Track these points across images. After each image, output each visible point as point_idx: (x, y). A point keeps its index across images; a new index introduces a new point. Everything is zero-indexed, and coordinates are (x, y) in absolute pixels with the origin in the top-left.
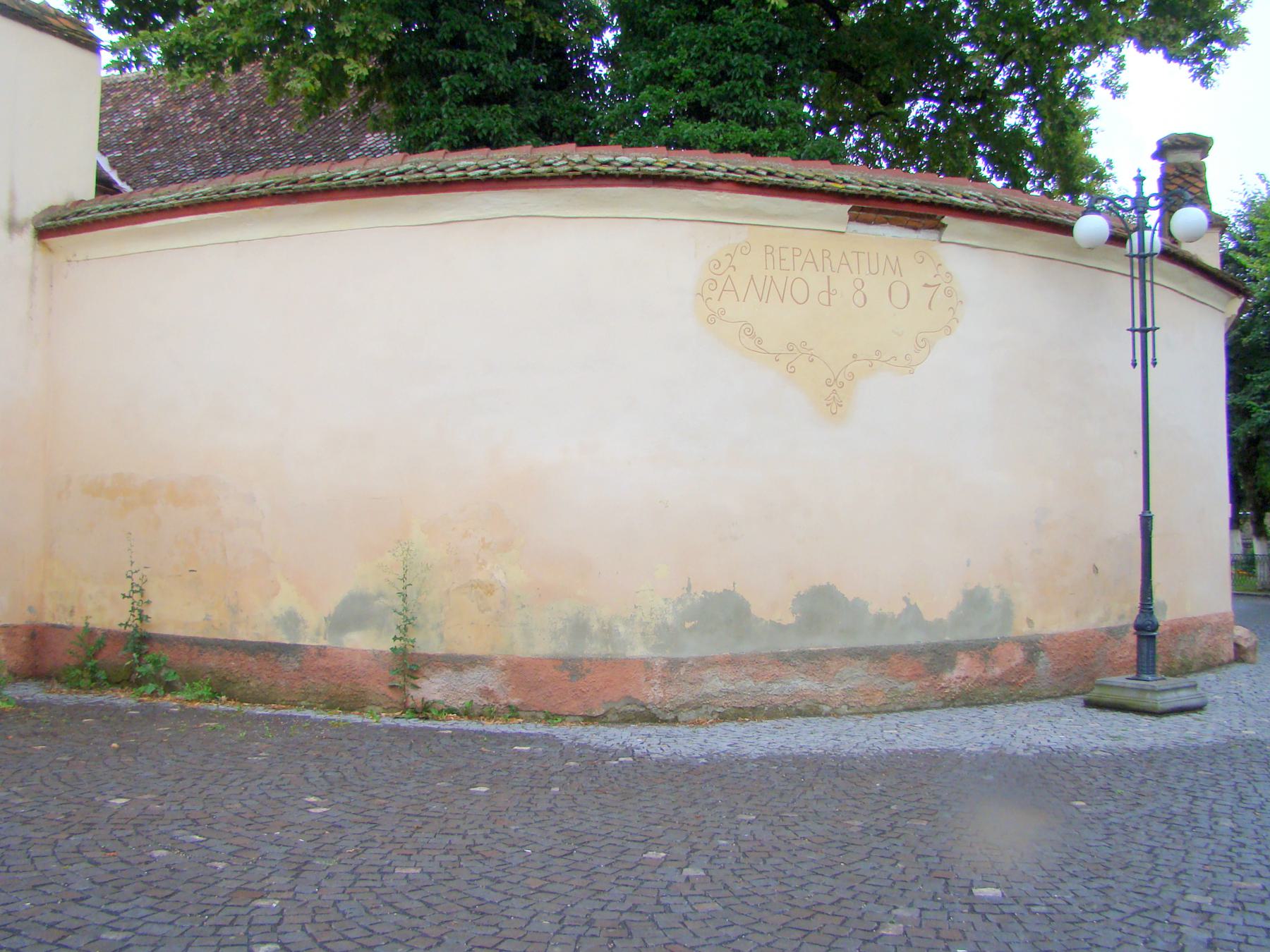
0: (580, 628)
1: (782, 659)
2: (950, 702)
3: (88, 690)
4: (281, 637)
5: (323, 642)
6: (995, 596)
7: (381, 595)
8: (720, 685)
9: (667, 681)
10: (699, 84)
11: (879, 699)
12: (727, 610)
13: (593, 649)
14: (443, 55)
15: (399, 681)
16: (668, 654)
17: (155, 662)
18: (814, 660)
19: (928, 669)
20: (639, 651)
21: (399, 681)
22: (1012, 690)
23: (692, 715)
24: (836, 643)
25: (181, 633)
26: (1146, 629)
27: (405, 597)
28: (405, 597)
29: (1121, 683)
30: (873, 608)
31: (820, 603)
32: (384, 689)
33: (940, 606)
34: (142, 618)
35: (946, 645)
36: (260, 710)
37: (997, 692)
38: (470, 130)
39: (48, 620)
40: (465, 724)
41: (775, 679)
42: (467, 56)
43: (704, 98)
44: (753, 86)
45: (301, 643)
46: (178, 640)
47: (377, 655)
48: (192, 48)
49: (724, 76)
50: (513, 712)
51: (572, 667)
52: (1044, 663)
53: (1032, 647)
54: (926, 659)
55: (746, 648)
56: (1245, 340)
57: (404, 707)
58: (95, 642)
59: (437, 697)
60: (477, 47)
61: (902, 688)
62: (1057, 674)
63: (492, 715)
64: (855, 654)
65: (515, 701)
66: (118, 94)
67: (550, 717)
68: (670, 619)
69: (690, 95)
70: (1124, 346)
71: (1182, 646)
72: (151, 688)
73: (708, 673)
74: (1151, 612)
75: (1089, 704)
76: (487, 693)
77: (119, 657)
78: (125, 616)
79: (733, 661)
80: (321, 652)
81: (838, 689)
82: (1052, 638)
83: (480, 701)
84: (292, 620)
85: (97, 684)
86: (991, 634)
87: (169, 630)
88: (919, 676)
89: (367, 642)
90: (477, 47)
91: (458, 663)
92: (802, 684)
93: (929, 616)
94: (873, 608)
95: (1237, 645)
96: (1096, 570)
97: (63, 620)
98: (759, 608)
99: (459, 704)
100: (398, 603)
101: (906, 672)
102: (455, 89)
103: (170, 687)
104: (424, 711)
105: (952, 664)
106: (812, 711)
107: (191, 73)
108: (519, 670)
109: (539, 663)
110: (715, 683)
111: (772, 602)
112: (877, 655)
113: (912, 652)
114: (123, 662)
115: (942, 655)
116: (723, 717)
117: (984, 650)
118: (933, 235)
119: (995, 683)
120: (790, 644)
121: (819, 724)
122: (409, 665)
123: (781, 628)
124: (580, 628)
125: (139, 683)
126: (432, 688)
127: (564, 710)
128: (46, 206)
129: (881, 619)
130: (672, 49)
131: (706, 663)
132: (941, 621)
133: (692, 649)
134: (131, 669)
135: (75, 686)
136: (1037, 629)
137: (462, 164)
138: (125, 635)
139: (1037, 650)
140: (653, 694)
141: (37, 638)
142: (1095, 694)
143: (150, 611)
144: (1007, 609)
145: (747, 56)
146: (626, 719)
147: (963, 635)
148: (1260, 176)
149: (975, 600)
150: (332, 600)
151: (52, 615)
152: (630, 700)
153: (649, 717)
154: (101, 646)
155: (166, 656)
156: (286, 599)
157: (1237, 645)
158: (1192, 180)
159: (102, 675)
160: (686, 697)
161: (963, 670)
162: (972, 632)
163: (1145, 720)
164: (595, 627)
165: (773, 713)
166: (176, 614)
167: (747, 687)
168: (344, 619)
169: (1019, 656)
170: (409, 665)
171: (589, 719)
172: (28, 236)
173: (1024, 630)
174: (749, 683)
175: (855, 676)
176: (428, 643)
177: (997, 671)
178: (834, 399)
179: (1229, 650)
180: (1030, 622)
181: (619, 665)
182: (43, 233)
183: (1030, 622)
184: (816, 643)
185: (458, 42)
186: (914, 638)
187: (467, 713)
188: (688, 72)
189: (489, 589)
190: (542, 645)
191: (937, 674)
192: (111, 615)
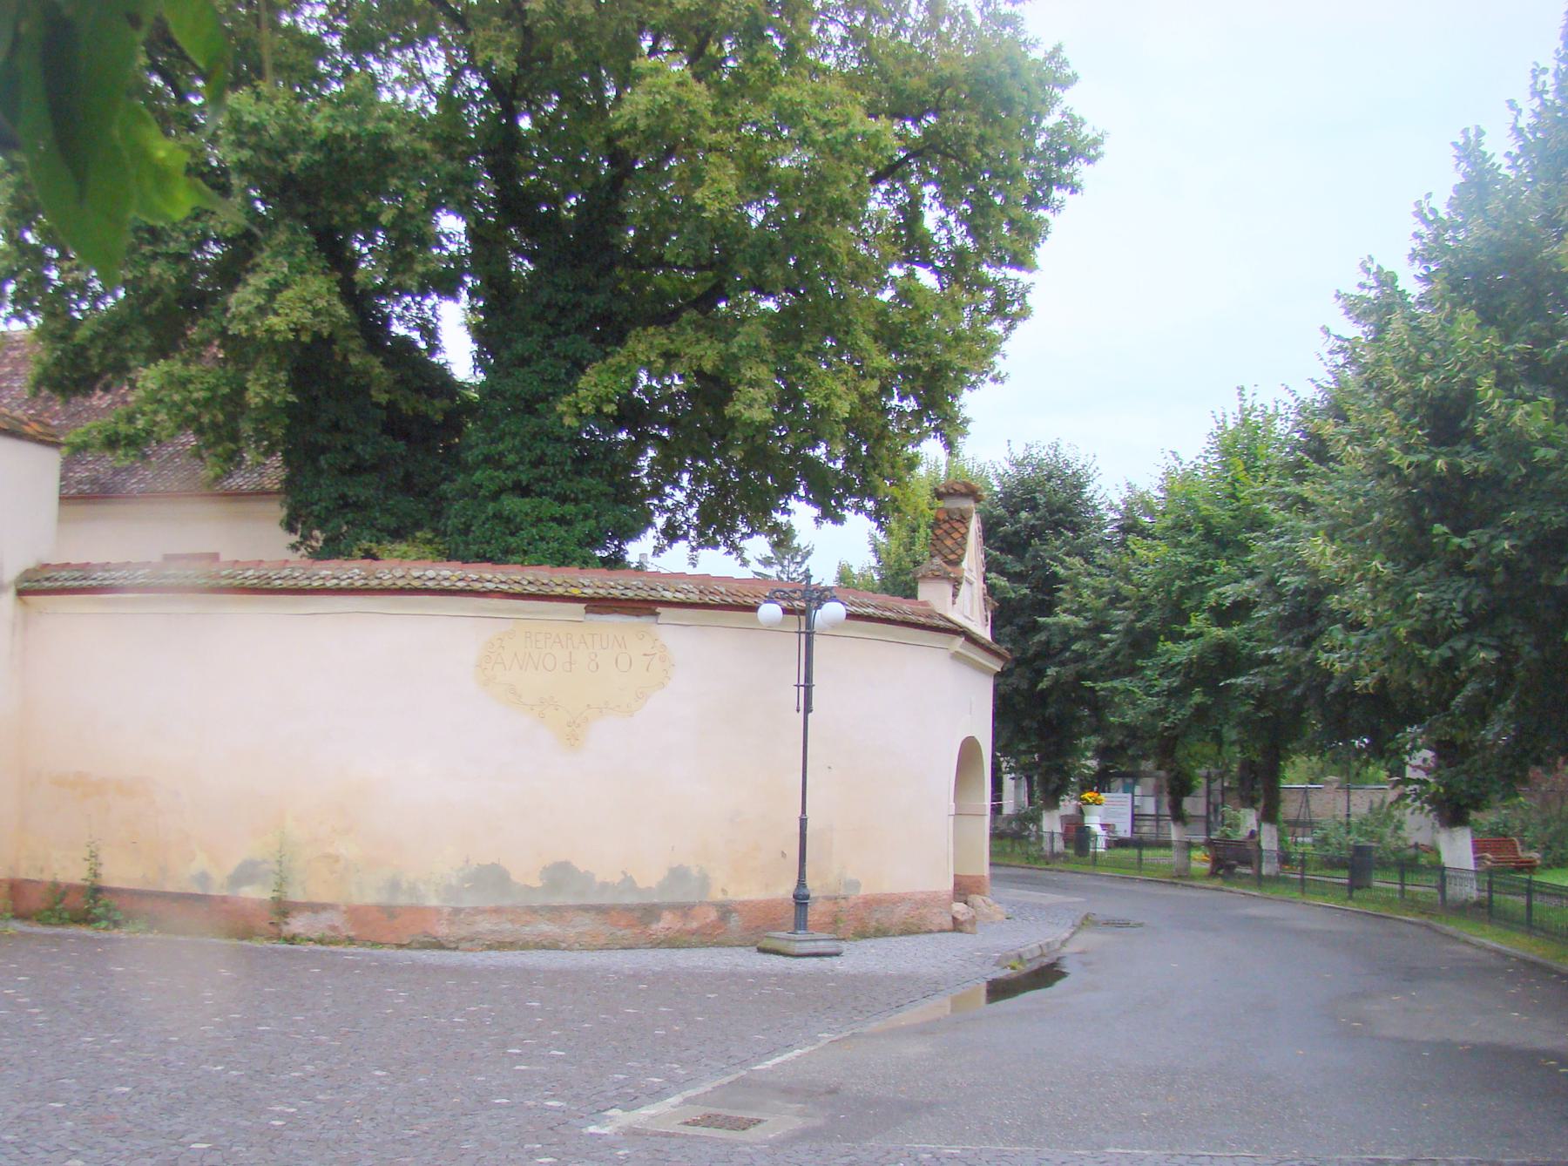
0: (395, 885)
1: (533, 911)
2: (656, 945)
3: (57, 925)
4: (196, 889)
5: (225, 893)
6: (694, 872)
7: (265, 861)
8: (488, 926)
9: (451, 923)
10: (521, 468)
11: (602, 941)
12: (494, 876)
13: (403, 900)
14: (322, 439)
15: (276, 919)
16: (453, 904)
17: (106, 906)
18: (556, 912)
19: (636, 920)
20: (433, 901)
21: (276, 919)
22: (708, 938)
23: (468, 945)
24: (571, 901)
25: (125, 886)
26: (801, 900)
27: (280, 863)
28: (280, 863)
29: (780, 937)
30: (599, 878)
31: (559, 874)
32: (265, 924)
33: (650, 878)
34: (96, 875)
35: (654, 905)
36: (181, 938)
37: (694, 939)
38: (343, 497)
39: (22, 876)
40: (319, 947)
41: (527, 923)
42: (340, 440)
43: (524, 478)
44: (562, 471)
45: (211, 893)
46: (122, 890)
47: (262, 902)
48: (127, 436)
49: (539, 462)
50: (351, 941)
51: (390, 912)
52: (735, 921)
53: (725, 910)
54: (638, 914)
55: (506, 902)
56: (1138, 625)
57: (279, 937)
58: (60, 892)
59: (301, 930)
60: (350, 431)
61: (620, 933)
62: (746, 929)
63: (337, 943)
64: (586, 909)
65: (352, 934)
66: (16, 354)
67: (375, 944)
68: (454, 882)
69: (513, 476)
70: (792, 696)
71: (878, 915)
72: (104, 924)
73: (479, 918)
74: (804, 886)
75: (763, 950)
76: (334, 928)
77: (81, 903)
78: (86, 874)
79: (498, 911)
80: (224, 899)
81: (572, 932)
82: (743, 903)
83: (329, 933)
84: (204, 878)
85: (62, 922)
86: (692, 899)
87: (115, 884)
88: (633, 926)
89: (256, 893)
90: (350, 431)
91: (315, 908)
92: (546, 928)
93: (641, 885)
94: (599, 878)
95: (954, 919)
96: (783, 854)
97: (33, 876)
98: (516, 876)
99: (315, 936)
100: (276, 868)
101: (623, 922)
102: (331, 465)
103: (116, 924)
104: (292, 940)
105: (658, 918)
106: (554, 946)
107: (126, 455)
108: (356, 914)
109: (367, 909)
110: (484, 925)
111: (526, 872)
112: (601, 910)
113: (628, 909)
114: (84, 907)
115: (649, 912)
116: (490, 947)
117: (685, 910)
118: (651, 619)
119: (693, 933)
120: (538, 901)
121: (552, 954)
122: (283, 909)
123: (531, 889)
124: (395, 885)
125: (93, 921)
126: (297, 925)
127: (384, 940)
128: (22, 569)
129: (604, 886)
130: (501, 438)
131: (479, 911)
132: (650, 888)
133: (468, 902)
134: (88, 912)
135: (45, 922)
136: (731, 896)
137: (324, 573)
138: (83, 888)
139: (730, 912)
140: (442, 930)
141: (16, 888)
142: (760, 945)
143: (103, 871)
144: (705, 882)
145: (559, 446)
146: (425, 946)
147: (667, 898)
148: (1174, 453)
149: (678, 875)
150: (232, 864)
151: (26, 872)
152: (426, 934)
153: (439, 945)
154: (65, 894)
155: (115, 902)
156: (200, 863)
157: (954, 919)
158: (957, 525)
159: (66, 915)
160: (463, 933)
161: (666, 923)
162: (678, 897)
163: (781, 958)
164: (405, 886)
165: (525, 946)
166: (119, 873)
167: (507, 928)
168: (239, 878)
169: (713, 915)
170: (283, 909)
171: (400, 946)
172: (10, 595)
173: (718, 896)
174: (509, 926)
175: (586, 924)
176: (295, 894)
177: (695, 925)
178: (573, 735)
179: (948, 923)
180: (724, 891)
181: (418, 911)
182: (21, 593)
183: (724, 891)
184: (557, 900)
185: (335, 427)
186: (630, 899)
187: (321, 941)
188: (511, 458)
189: (337, 859)
190: (370, 896)
191: (647, 925)
192: (72, 872)
